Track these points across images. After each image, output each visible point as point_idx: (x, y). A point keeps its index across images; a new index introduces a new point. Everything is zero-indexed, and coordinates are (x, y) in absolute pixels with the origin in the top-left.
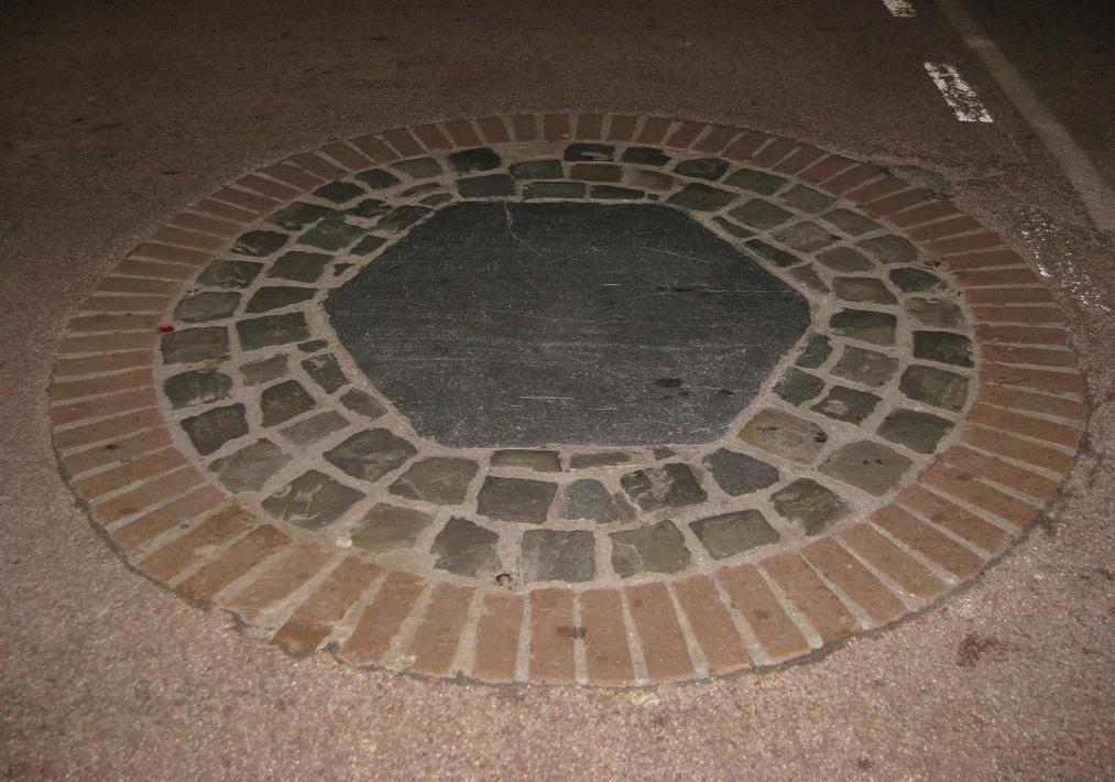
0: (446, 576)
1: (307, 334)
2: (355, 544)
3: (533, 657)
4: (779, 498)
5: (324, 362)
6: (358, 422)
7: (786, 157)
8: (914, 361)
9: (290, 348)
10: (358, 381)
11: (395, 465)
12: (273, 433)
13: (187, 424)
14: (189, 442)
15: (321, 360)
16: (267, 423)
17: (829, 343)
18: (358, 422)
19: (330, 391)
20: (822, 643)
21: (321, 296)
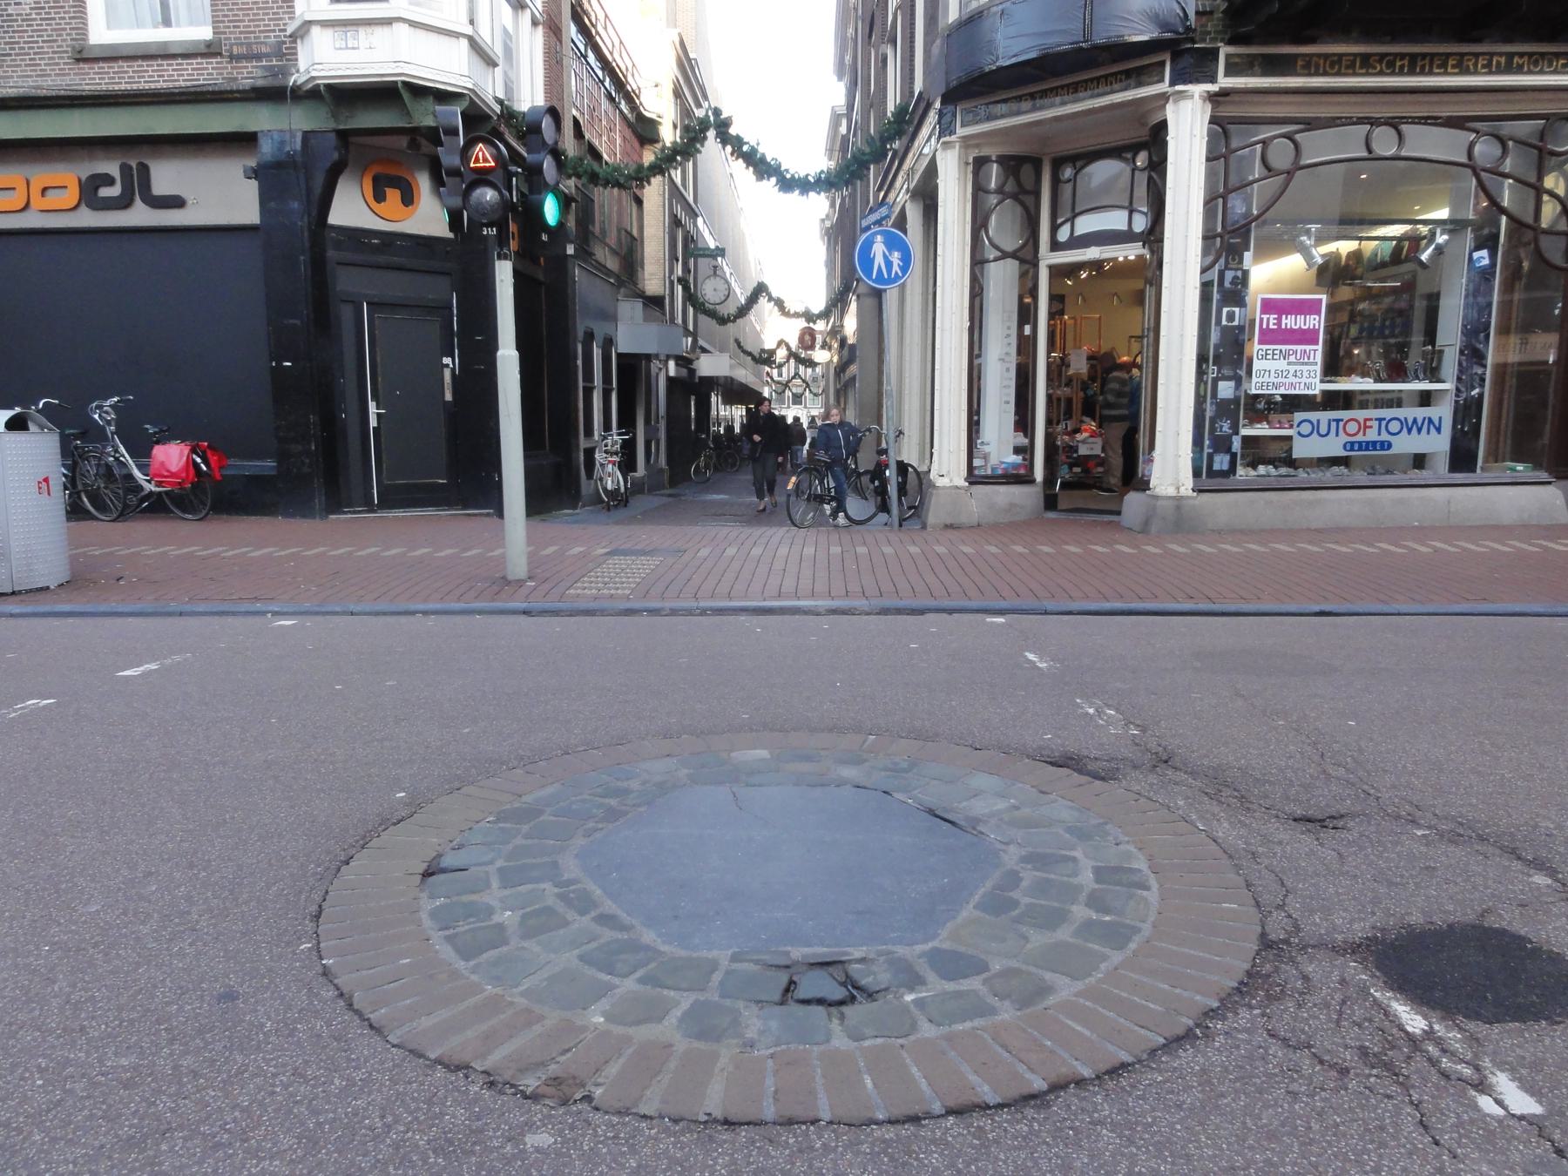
2: (607, 1020)
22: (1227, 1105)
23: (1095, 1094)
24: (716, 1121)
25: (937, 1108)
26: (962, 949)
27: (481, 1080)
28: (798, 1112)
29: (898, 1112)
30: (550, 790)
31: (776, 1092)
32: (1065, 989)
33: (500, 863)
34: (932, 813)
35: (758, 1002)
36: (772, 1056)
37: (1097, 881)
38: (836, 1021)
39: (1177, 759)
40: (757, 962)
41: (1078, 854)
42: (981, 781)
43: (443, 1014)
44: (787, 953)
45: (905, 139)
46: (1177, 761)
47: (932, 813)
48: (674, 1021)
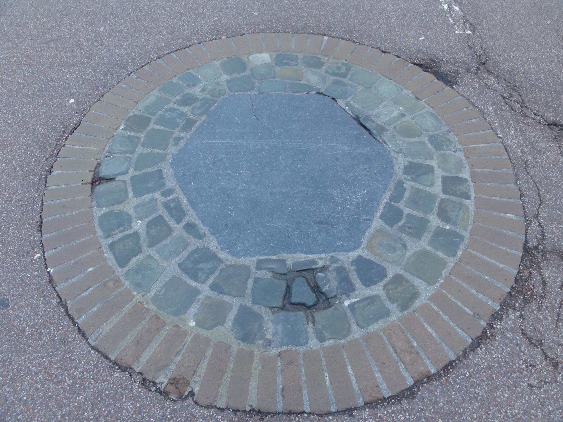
0: (243, 346)
1: (164, 185)
2: (197, 324)
3: (163, 376)
4: (388, 287)
5: (174, 203)
6: (195, 243)
7: (426, 325)
8: (443, 196)
9: (157, 195)
10: (192, 216)
11: (211, 272)
12: (152, 252)
13: (112, 247)
14: (403, 389)
15: (172, 202)
16: (151, 245)
17: (404, 185)
18: (195, 243)
19: (178, 222)
20: (413, 382)
21: (169, 159)
22: (498, 397)
23: (437, 387)
24: (253, 410)
25: (361, 403)
26: (373, 258)
27: (138, 378)
28: (295, 409)
29: (342, 407)
30: (151, 99)
31: (283, 388)
32: (426, 292)
33: (132, 172)
34: (357, 119)
35: (272, 308)
36: (280, 355)
37: (445, 191)
38: (311, 324)
39: (490, 62)
40: (270, 270)
41: (434, 163)
42: (386, 87)
43: (114, 320)
44: (284, 261)
45: (330, 337)
46: (489, 65)
47: (357, 119)
48: (230, 324)
